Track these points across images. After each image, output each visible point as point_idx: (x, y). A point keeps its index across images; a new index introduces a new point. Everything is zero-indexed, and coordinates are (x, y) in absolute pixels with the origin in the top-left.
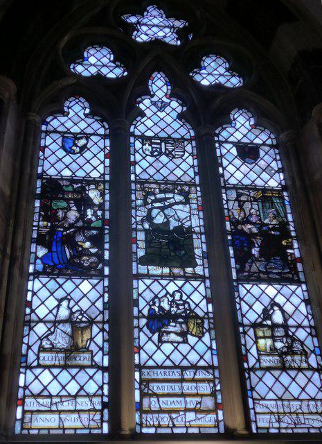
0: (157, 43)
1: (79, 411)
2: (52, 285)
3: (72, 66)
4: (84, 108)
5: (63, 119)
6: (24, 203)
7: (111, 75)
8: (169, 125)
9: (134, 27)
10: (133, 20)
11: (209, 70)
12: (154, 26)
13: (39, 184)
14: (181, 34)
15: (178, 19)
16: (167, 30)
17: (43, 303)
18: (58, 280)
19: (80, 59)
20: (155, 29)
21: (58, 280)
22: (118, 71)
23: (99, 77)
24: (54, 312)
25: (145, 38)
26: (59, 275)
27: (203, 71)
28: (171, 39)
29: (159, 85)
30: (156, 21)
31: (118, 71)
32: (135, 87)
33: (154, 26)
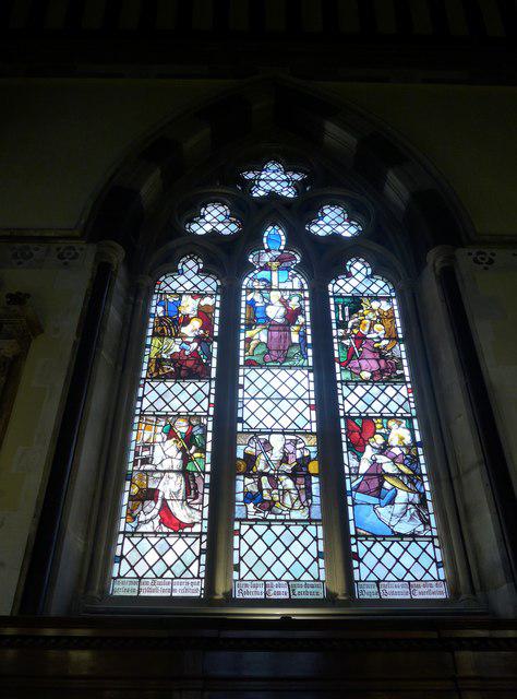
0: (272, 195)
1: (279, 290)
2: (177, 388)
3: (187, 226)
4: (198, 264)
5: (182, 279)
6: (462, 578)
7: (226, 232)
8: (161, 557)
9: (251, 183)
10: (251, 176)
11: (327, 219)
12: (272, 180)
13: (152, 320)
14: (297, 186)
15: (295, 172)
16: (285, 184)
17: (160, 396)
18: (296, 427)
19: (196, 216)
20: (273, 184)
21: (296, 427)
22: (234, 227)
23: (214, 234)
24: (292, 402)
25: (262, 193)
26: (184, 379)
27: (320, 222)
28: (289, 193)
29: (275, 237)
30: (273, 176)
31: (234, 227)
32: (249, 238)
33: (272, 180)
